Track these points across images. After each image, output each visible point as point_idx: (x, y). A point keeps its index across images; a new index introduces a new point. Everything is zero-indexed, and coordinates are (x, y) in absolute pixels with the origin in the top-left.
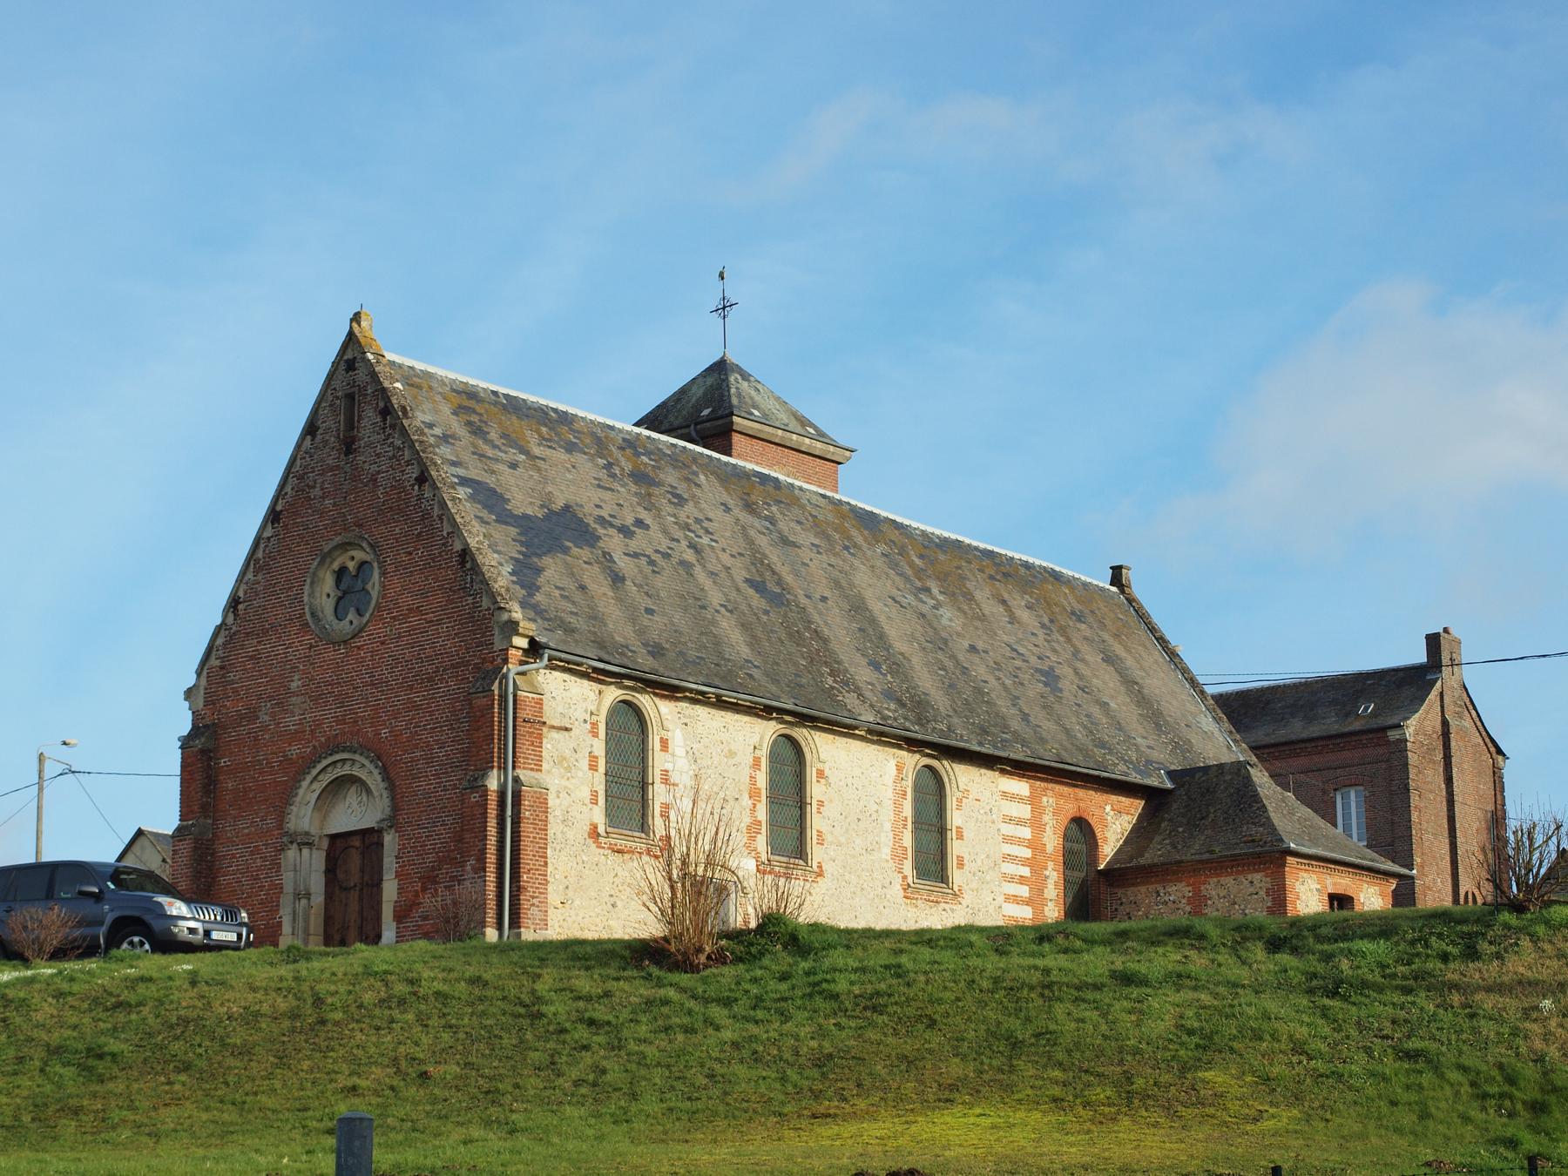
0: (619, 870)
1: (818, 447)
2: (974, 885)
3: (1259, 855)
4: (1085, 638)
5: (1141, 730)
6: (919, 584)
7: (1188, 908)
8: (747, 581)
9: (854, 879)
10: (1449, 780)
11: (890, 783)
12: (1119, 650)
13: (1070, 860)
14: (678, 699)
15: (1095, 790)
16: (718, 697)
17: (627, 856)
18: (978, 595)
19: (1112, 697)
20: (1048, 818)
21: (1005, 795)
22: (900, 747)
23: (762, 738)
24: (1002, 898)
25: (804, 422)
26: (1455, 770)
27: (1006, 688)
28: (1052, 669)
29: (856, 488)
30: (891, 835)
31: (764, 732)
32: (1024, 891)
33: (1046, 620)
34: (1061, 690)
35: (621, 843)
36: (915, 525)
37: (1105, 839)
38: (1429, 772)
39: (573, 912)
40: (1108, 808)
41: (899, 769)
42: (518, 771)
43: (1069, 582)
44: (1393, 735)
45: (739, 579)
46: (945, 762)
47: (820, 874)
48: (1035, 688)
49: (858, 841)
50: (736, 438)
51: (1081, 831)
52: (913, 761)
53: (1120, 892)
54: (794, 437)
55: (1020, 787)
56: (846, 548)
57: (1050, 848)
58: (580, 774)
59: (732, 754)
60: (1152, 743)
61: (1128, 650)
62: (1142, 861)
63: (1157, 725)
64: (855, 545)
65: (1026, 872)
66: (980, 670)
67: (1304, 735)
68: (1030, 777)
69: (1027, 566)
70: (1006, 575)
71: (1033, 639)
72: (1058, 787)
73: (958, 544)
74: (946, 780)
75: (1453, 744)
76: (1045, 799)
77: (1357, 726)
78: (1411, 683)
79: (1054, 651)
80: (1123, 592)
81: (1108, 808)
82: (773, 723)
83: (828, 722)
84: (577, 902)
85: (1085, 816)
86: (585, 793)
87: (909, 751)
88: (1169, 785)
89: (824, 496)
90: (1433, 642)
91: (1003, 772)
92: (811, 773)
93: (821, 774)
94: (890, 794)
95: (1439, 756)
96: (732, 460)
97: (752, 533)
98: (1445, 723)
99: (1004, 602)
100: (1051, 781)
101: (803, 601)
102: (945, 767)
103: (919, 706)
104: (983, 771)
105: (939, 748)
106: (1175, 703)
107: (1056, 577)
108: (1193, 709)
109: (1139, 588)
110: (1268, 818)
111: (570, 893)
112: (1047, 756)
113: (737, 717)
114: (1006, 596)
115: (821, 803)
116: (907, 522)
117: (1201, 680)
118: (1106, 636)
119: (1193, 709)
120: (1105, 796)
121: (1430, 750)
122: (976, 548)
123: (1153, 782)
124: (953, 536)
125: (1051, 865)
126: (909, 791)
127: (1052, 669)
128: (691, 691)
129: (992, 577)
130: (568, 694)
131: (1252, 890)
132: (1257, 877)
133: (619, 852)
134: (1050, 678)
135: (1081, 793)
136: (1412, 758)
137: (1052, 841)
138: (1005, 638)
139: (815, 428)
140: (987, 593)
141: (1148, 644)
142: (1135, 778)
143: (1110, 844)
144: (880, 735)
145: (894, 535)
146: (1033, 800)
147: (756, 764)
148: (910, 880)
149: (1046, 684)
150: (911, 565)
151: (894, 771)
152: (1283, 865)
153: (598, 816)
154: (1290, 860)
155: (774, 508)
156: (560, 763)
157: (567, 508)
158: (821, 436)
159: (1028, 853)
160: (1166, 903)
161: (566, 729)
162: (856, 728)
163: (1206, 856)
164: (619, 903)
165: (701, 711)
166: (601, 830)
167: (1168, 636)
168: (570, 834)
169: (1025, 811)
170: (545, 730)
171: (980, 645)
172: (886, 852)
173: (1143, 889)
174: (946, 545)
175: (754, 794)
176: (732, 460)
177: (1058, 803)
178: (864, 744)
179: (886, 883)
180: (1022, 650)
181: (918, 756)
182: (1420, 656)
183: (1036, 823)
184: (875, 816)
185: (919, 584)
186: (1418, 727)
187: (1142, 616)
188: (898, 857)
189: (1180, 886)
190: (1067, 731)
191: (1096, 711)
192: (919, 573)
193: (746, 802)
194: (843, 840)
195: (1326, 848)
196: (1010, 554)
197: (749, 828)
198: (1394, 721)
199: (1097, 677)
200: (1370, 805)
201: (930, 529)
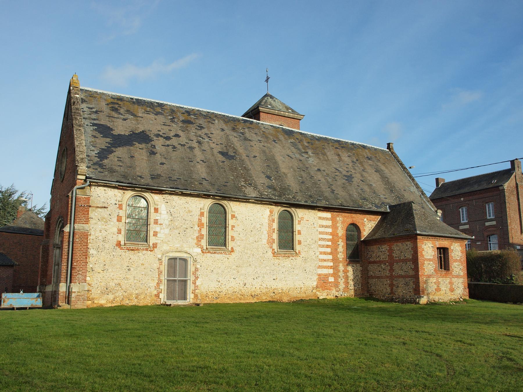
0: (132, 257)
1: (291, 115)
2: (306, 250)
3: (408, 236)
4: (370, 165)
5: (383, 193)
6: (303, 151)
7: (388, 254)
8: (220, 152)
9: (249, 252)
10: (518, 199)
11: (267, 218)
12: (383, 168)
13: (349, 238)
14: (163, 194)
15: (360, 214)
16: (182, 192)
17: (136, 251)
18: (328, 154)
19: (375, 183)
20: (339, 225)
21: (320, 218)
22: (271, 205)
23: (204, 205)
24: (319, 253)
25: (288, 108)
26: (520, 196)
27: (328, 182)
28: (351, 175)
29: (306, 128)
30: (267, 235)
31: (207, 203)
32: (329, 250)
33: (355, 160)
34: (352, 182)
35: (132, 247)
36: (309, 133)
37: (364, 230)
38: (512, 197)
39: (108, 274)
40: (365, 220)
41: (271, 212)
42: (76, 226)
43: (369, 149)
44: (501, 188)
45: (215, 151)
46: (293, 209)
47: (232, 250)
48: (341, 181)
49: (251, 238)
50: (261, 114)
51: (354, 228)
52: (277, 210)
53: (369, 247)
54: (282, 112)
55: (328, 215)
56: (274, 141)
57: (340, 235)
58: (112, 223)
59: (190, 211)
60: (387, 197)
61: (387, 168)
62: (374, 237)
63: (392, 191)
64: (279, 140)
65: (330, 243)
66: (319, 176)
67: (477, 189)
68: (331, 211)
69: (353, 144)
70: (342, 147)
71: (347, 166)
72: (343, 214)
73: (326, 139)
74: (293, 215)
75: (519, 189)
76: (338, 218)
77: (491, 186)
78: (506, 174)
79: (355, 169)
80: (390, 151)
81: (365, 220)
82: (210, 200)
83: (229, 198)
84: (110, 270)
85: (355, 223)
86: (115, 230)
87: (275, 206)
88: (389, 211)
89: (271, 126)
90: (512, 162)
91: (319, 210)
92: (229, 216)
93: (233, 216)
94: (267, 221)
95: (515, 193)
96: (261, 122)
97: (231, 137)
98: (517, 184)
99: (339, 155)
100: (341, 212)
101: (244, 157)
102: (293, 210)
103: (284, 190)
104: (310, 211)
105: (286, 202)
106: (401, 183)
107: (364, 147)
108: (409, 185)
109: (397, 150)
110: (414, 222)
111: (106, 267)
112: (335, 204)
113: (192, 198)
114: (340, 153)
115: (233, 226)
116: (306, 133)
117: (413, 176)
118: (379, 164)
119: (409, 185)
120: (364, 216)
121: (512, 191)
122: (333, 140)
123: (382, 210)
124: (324, 136)
125: (340, 240)
126: (276, 220)
127: (351, 175)
128: (168, 191)
129: (336, 148)
130: (107, 195)
131: (407, 248)
132: (408, 243)
133: (131, 250)
134: (349, 178)
135: (354, 215)
136: (506, 194)
137: (341, 232)
138: (335, 166)
139: (291, 109)
140: (333, 152)
141: (396, 166)
142: (374, 209)
143: (365, 233)
144: (260, 201)
145: (299, 137)
146: (333, 219)
147: (202, 214)
148: (276, 250)
149: (346, 180)
150: (303, 145)
151: (269, 213)
152: (417, 239)
153: (121, 238)
154: (418, 237)
155: (246, 130)
156: (102, 220)
157: (143, 131)
158: (293, 112)
159: (331, 237)
160: (381, 252)
161: (105, 207)
162: (249, 200)
163: (392, 236)
164: (132, 269)
165: (175, 198)
166: (122, 243)
167: (404, 163)
168: (107, 246)
169: (330, 223)
170: (90, 209)
171: (322, 169)
172: (265, 241)
173: (375, 246)
174: (320, 139)
175: (200, 225)
176: (261, 122)
177: (343, 221)
178: (254, 205)
179: (265, 252)
180: (340, 169)
181: (280, 207)
182: (508, 166)
183: (334, 227)
184: (259, 229)
185: (303, 151)
186: (508, 185)
187: (396, 157)
188: (270, 242)
189: (386, 246)
190: (350, 195)
191: (366, 188)
192: (305, 147)
193: (196, 228)
194: (244, 238)
195: (436, 231)
196: (347, 141)
197: (197, 238)
198: (500, 184)
199: (370, 177)
200: (495, 208)
201: (315, 135)
